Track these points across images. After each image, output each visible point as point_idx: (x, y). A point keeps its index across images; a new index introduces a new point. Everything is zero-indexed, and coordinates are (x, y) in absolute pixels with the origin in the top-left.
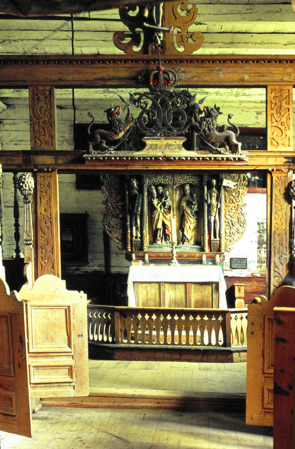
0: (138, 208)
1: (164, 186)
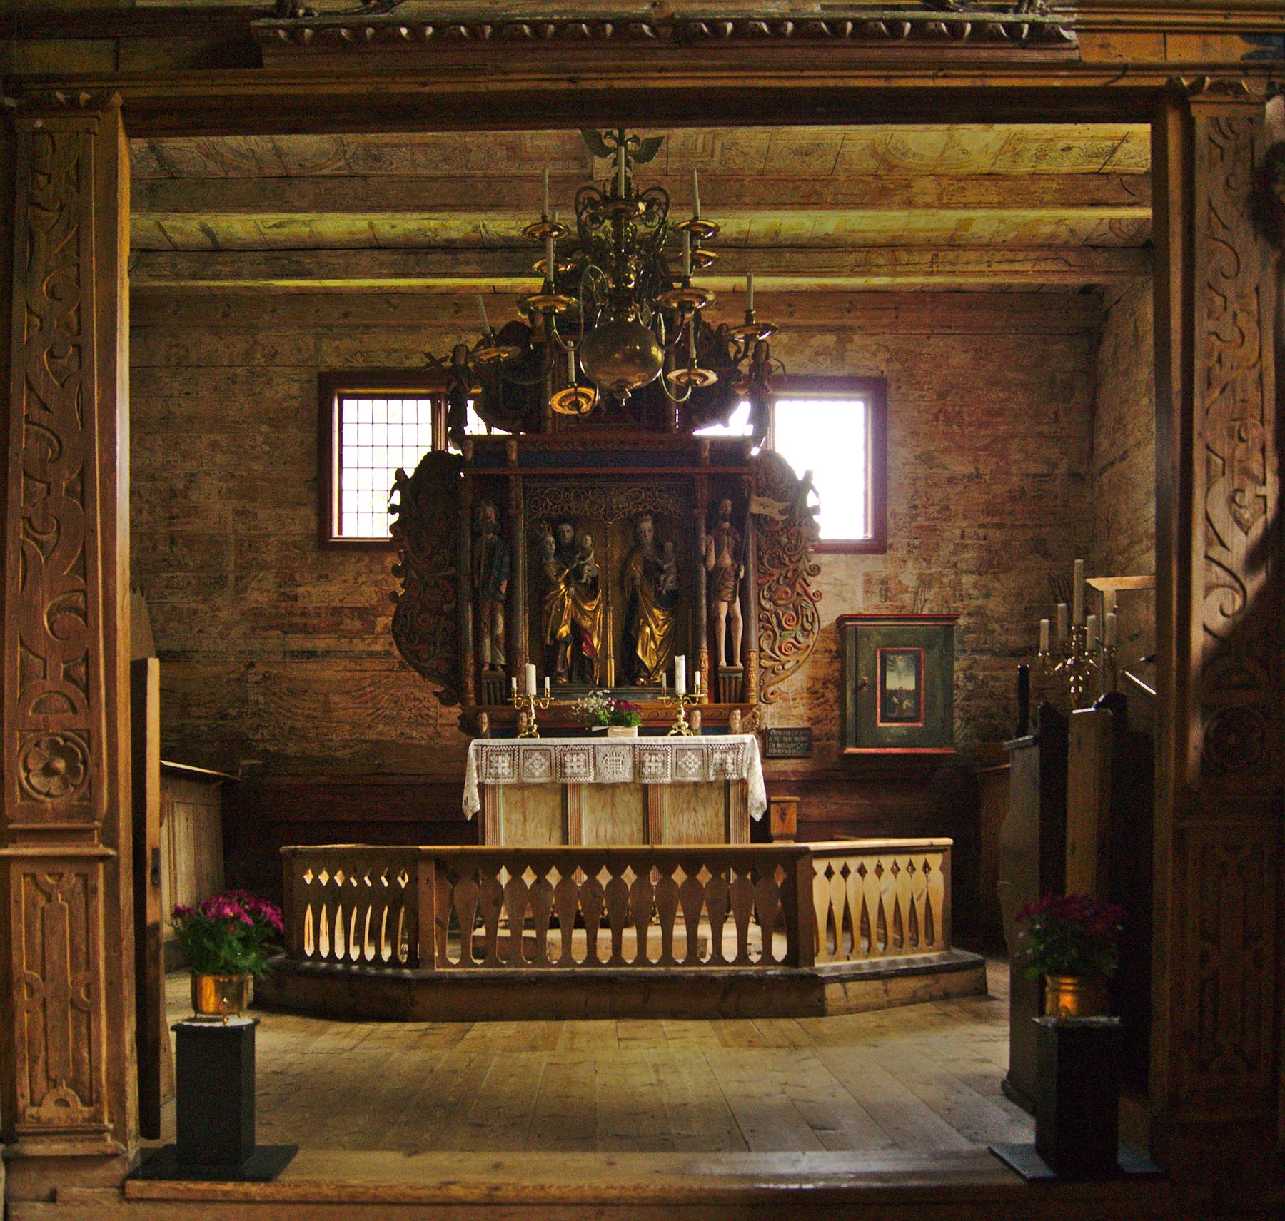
1: (575, 522)
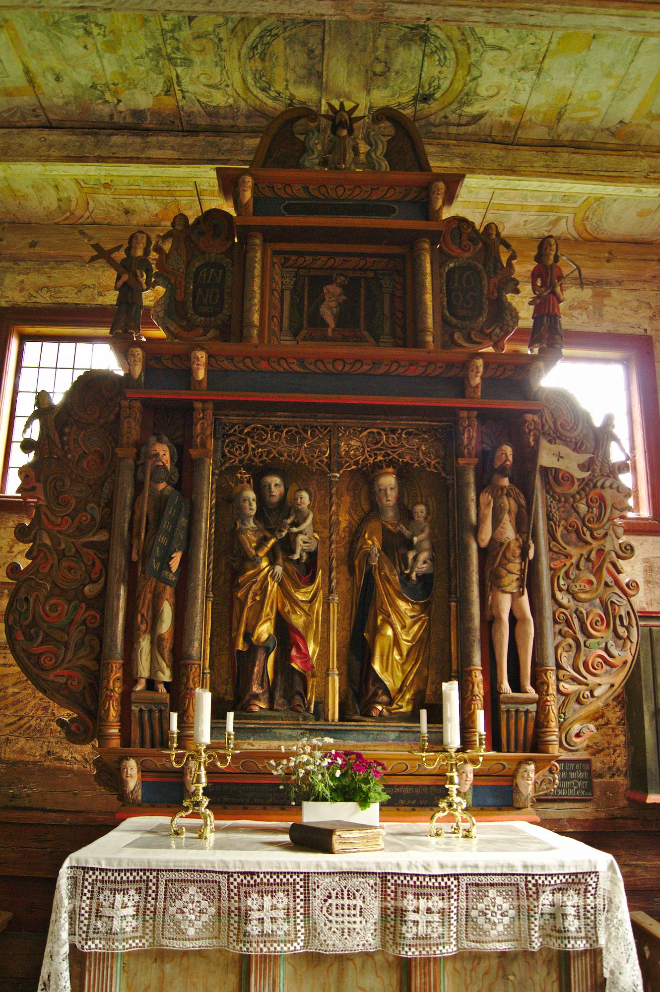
0: (166, 558)
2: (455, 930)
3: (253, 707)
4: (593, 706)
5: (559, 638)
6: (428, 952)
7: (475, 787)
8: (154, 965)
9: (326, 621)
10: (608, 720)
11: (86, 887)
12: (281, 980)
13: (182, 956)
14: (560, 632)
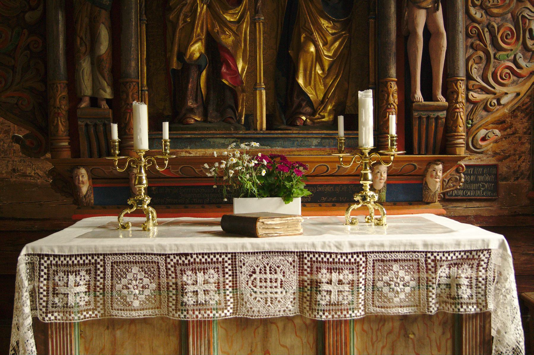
2: (363, 298)
3: (188, 120)
4: (499, 113)
5: (471, 51)
6: (339, 316)
7: (388, 185)
8: (107, 332)
9: (253, 40)
10: (516, 130)
11: (43, 271)
12: (215, 340)
13: (130, 324)
14: (472, 46)
